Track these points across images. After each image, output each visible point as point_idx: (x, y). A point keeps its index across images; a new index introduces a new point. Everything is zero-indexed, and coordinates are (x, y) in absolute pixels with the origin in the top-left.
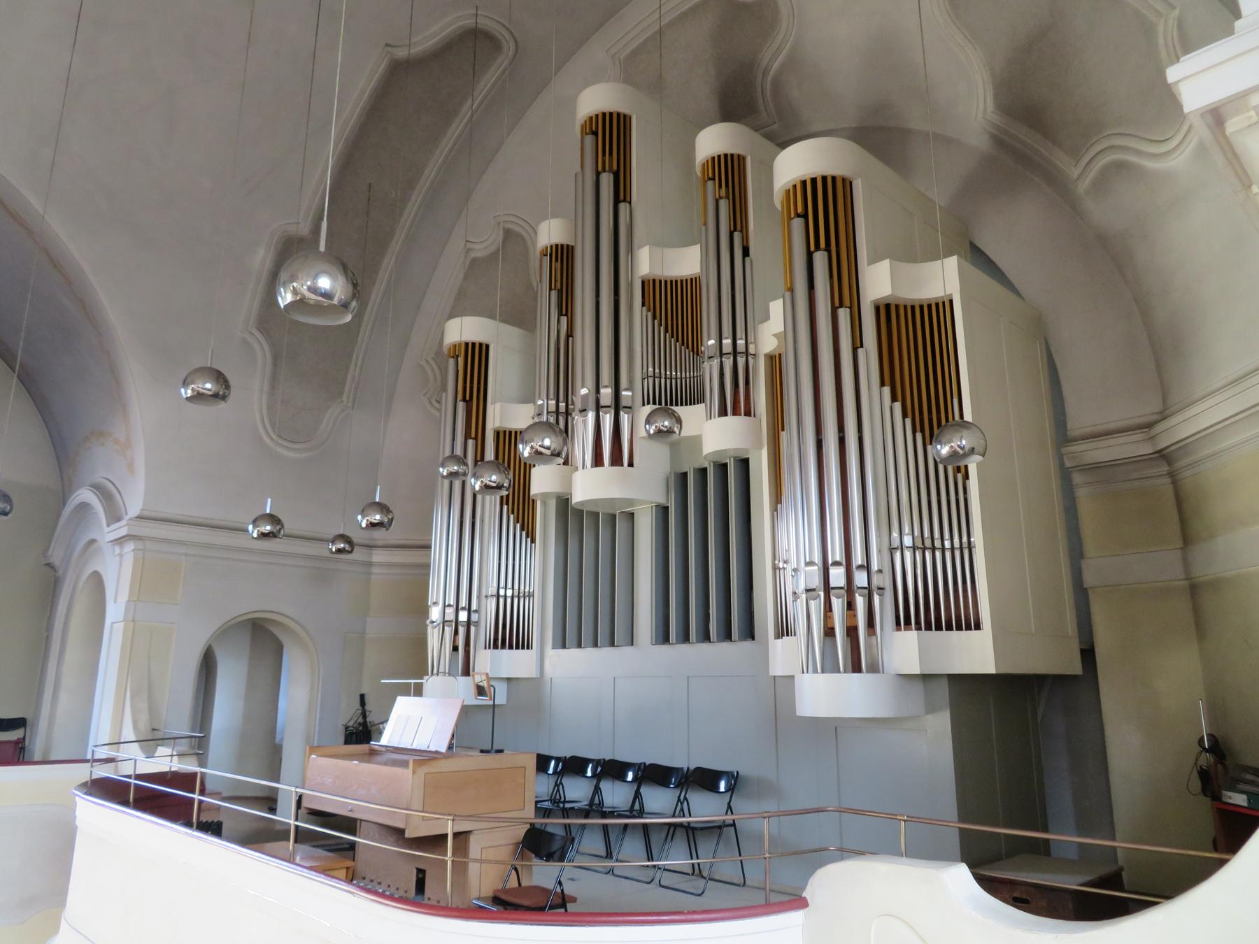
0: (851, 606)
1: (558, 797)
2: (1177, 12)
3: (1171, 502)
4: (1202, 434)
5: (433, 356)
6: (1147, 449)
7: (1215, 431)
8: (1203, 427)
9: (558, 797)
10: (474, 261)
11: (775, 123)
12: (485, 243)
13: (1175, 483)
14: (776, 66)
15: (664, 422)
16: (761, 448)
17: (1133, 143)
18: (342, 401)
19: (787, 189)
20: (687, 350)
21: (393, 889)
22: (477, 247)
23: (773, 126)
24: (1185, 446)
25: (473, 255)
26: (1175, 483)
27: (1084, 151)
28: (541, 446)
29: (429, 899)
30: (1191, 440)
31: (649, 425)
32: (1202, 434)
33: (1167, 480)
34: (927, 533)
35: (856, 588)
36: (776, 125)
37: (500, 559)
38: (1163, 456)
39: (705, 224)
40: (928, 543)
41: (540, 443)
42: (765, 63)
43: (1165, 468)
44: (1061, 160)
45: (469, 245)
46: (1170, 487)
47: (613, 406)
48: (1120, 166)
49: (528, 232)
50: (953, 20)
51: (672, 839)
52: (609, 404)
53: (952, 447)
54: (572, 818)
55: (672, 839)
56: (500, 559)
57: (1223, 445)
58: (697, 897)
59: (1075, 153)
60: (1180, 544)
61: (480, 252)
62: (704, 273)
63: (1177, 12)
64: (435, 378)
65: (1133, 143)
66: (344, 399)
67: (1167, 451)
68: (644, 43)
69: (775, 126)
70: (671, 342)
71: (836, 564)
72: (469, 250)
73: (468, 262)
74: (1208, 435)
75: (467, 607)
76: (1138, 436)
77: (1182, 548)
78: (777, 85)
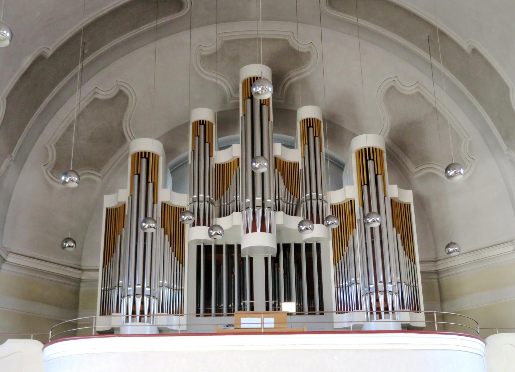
2: (471, 139)
5: (55, 144)
6: (434, 269)
10: (96, 99)
11: (283, 99)
14: (296, 79)
15: (335, 221)
18: (12, 156)
19: (358, 150)
20: (288, 191)
23: (281, 100)
25: (96, 96)
30: (443, 270)
33: (436, 281)
36: (282, 101)
38: (437, 272)
41: (376, 219)
42: (291, 76)
43: (436, 277)
44: (410, 164)
45: (97, 90)
46: (437, 283)
47: (262, 206)
48: (434, 175)
50: (384, 101)
53: (453, 249)
59: (417, 165)
60: (440, 301)
61: (103, 95)
63: (471, 139)
65: (434, 166)
66: (12, 155)
67: (439, 271)
68: (239, 40)
69: (282, 101)
71: (381, 282)
72: (95, 93)
73: (92, 98)
76: (432, 264)
77: (440, 303)
78: (290, 87)
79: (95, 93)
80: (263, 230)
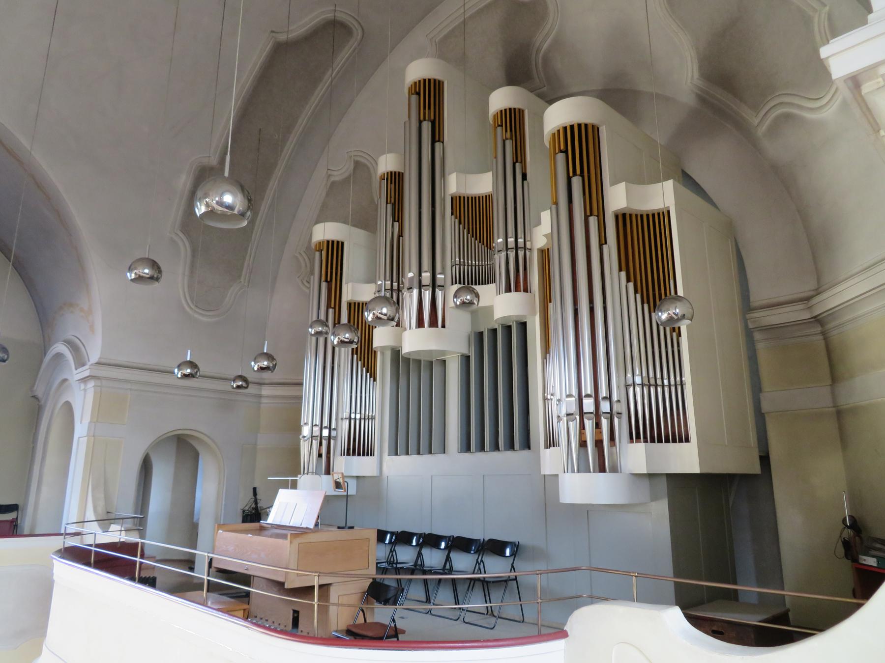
0: (598, 425)
1: (392, 559)
2: (827, 8)
3: (823, 353)
4: (845, 305)
5: (304, 250)
6: (806, 315)
7: (854, 303)
8: (846, 300)
9: (392, 559)
10: (333, 183)
11: (545, 86)
12: (341, 170)
13: (826, 339)
14: (545, 46)
15: (466, 296)
16: (535, 314)
17: (796, 101)
18: (241, 282)
19: (553, 132)
20: (483, 246)
21: (276, 625)
22: (335, 173)
23: (543, 89)
24: (833, 313)
25: (332, 179)
26: (826, 339)
27: (762, 106)
28: (381, 313)
29: (302, 631)
30: (837, 309)
31: (456, 299)
32: (845, 305)
33: (820, 337)
34: (651, 375)
35: (601, 413)
36: (545, 88)
37: (351, 393)
38: (818, 320)
39: (496, 157)
40: (652, 382)
41: (380, 311)
42: (537, 44)
43: (819, 329)
44: (746, 113)
45: (330, 172)
46: (823, 342)
47: (431, 285)
48: (788, 117)
49: (371, 163)
50: (670, 14)
51: (472, 589)
52: (428, 284)
54: (402, 574)
55: (472, 589)
56: (351, 393)
57: (860, 313)
58: (490, 630)
59: (756, 108)
60: (829, 382)
61: (337, 177)
62: (495, 192)
63: (827, 8)
64: (306, 266)
65: (796, 101)
66: (242, 280)
67: (821, 316)
68: (453, 31)
69: (545, 89)
70: (471, 240)
71: (588, 396)
72: (330, 176)
73: (329, 184)
74: (849, 305)
75: (328, 426)
76: (800, 306)
77: (831, 385)
78: (546, 60)
79: (330, 176)
80: (433, 323)
